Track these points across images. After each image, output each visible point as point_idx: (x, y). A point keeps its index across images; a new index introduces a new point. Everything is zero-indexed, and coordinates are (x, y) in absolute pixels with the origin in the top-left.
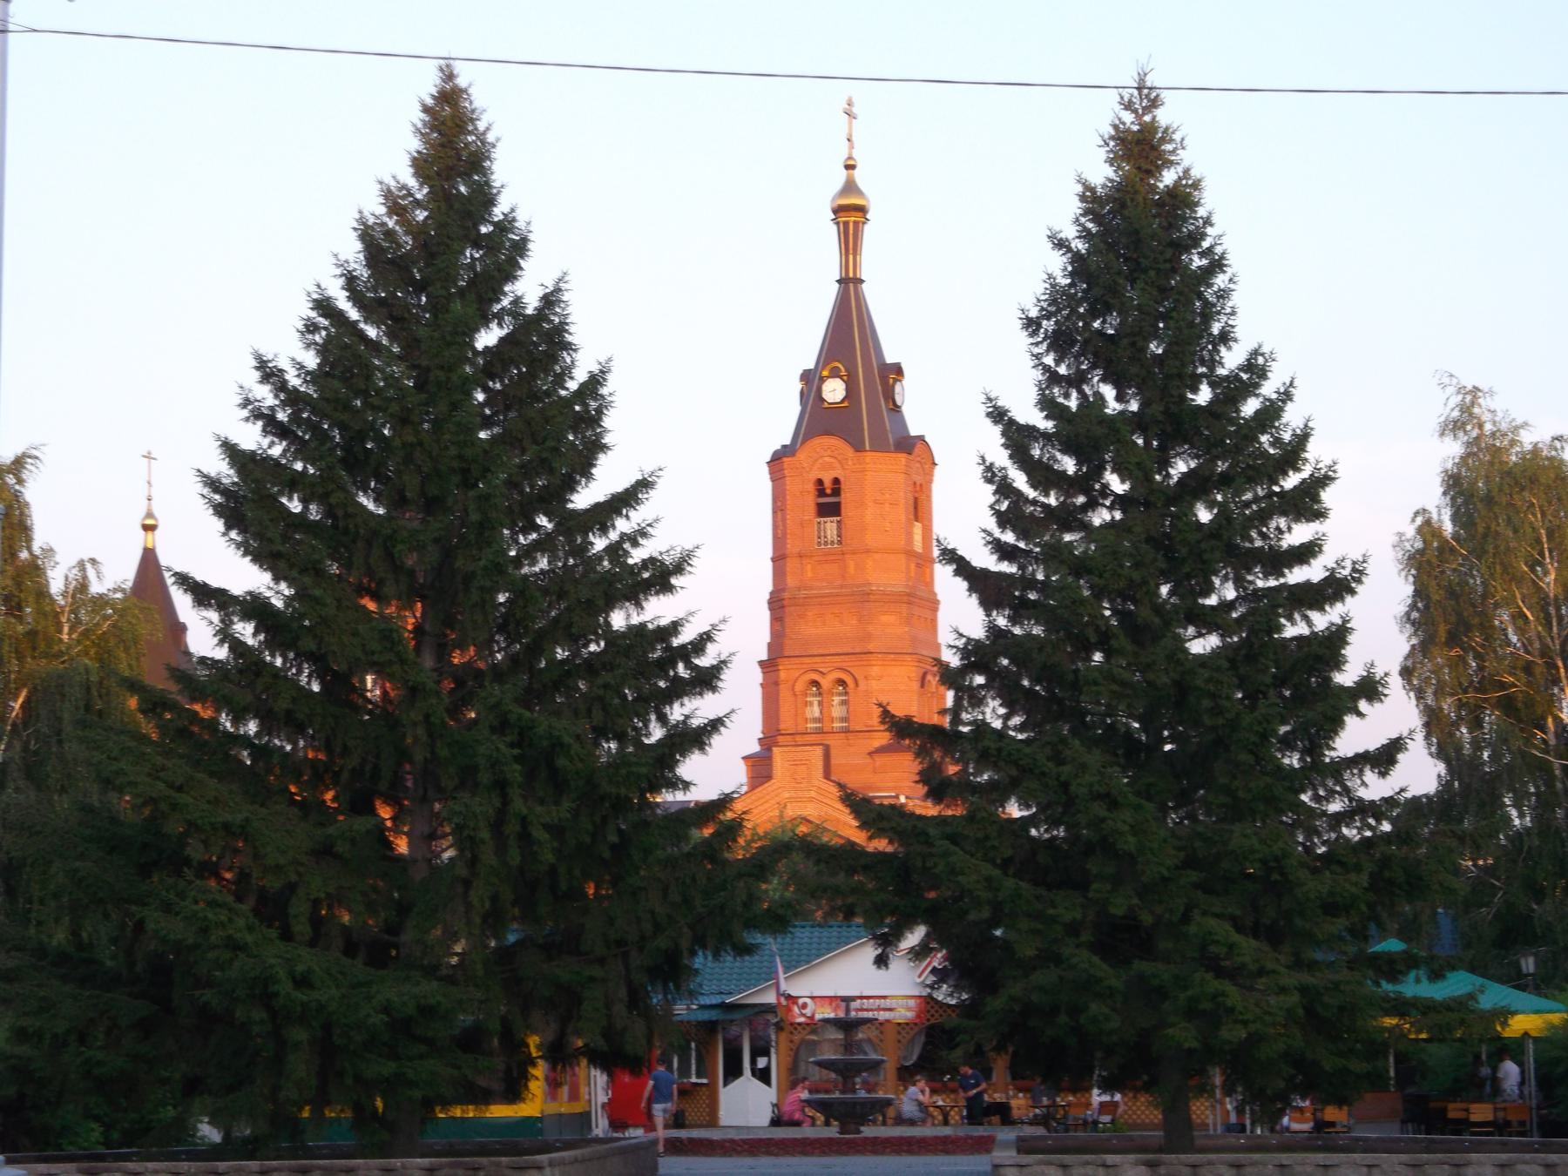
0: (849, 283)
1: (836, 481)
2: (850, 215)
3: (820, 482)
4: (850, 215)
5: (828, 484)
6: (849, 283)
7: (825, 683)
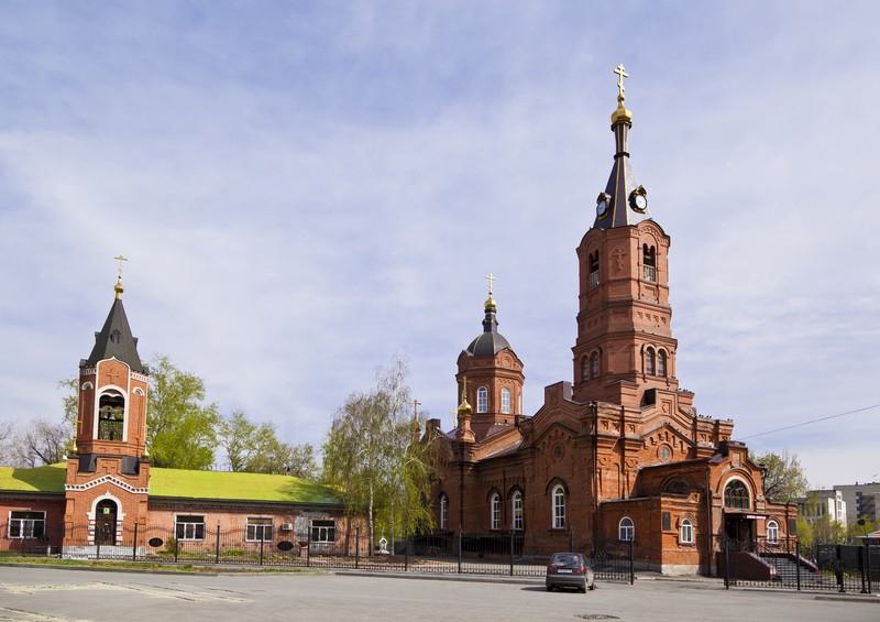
1: (597, 252)
6: (620, 154)
7: (656, 350)
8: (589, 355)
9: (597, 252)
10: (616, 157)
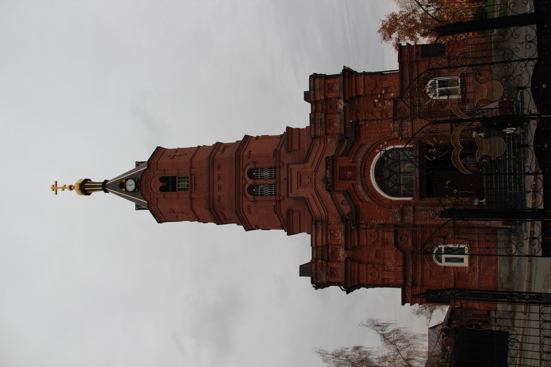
0: (105, 186)
1: (162, 179)
2: (86, 187)
3: (162, 189)
4: (86, 187)
5: (161, 184)
6: (105, 186)
7: (250, 182)
8: (250, 182)
9: (162, 179)
10: (106, 191)
